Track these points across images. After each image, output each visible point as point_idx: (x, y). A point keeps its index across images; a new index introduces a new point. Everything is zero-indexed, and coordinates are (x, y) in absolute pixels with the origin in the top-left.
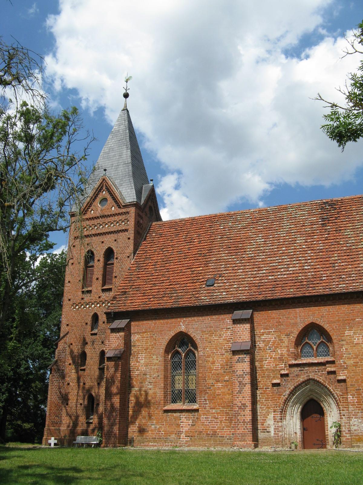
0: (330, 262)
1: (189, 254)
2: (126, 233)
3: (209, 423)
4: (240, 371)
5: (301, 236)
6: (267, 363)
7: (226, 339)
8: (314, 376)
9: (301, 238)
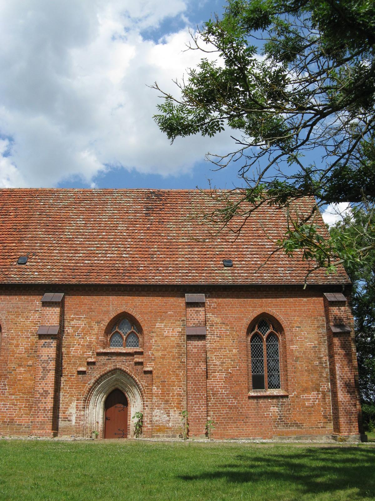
3: (7, 410)
6: (74, 350)
7: (34, 322)
8: (121, 366)
9: (123, 225)
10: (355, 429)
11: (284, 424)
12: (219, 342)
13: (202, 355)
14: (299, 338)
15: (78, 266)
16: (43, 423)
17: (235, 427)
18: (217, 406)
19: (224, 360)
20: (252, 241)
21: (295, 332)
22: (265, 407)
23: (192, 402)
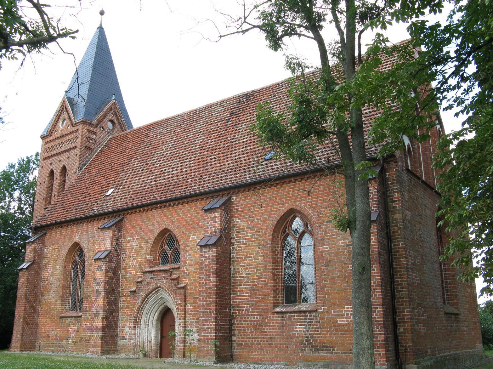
2: (75, 150)
6: (130, 271)
10: (381, 358)
11: (312, 347)
12: (244, 249)
14: (330, 236)
16: (96, 342)
17: (259, 349)
21: (325, 228)
22: (290, 325)
23: (203, 320)
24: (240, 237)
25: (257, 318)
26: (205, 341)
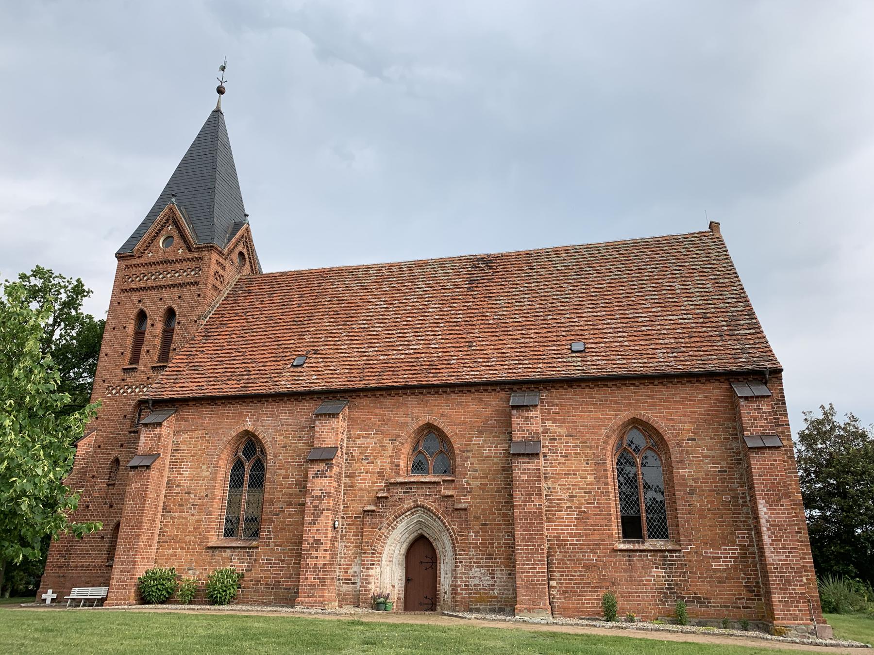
0: (467, 340)
1: (282, 321)
2: (196, 287)
3: (271, 567)
4: (317, 490)
5: (437, 302)
6: (361, 480)
8: (424, 502)
9: (436, 306)
11: (677, 597)
12: (564, 463)
13: (535, 484)
15: (369, 364)
18: (566, 564)
19: (574, 492)
20: (617, 312)
22: (643, 568)
23: (522, 557)
24: (557, 446)
25: (589, 556)
26: (528, 588)
